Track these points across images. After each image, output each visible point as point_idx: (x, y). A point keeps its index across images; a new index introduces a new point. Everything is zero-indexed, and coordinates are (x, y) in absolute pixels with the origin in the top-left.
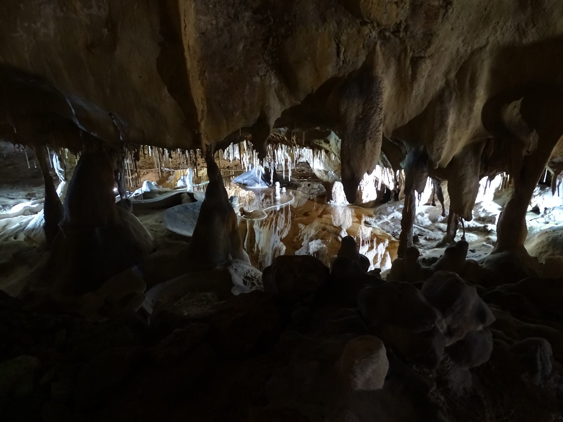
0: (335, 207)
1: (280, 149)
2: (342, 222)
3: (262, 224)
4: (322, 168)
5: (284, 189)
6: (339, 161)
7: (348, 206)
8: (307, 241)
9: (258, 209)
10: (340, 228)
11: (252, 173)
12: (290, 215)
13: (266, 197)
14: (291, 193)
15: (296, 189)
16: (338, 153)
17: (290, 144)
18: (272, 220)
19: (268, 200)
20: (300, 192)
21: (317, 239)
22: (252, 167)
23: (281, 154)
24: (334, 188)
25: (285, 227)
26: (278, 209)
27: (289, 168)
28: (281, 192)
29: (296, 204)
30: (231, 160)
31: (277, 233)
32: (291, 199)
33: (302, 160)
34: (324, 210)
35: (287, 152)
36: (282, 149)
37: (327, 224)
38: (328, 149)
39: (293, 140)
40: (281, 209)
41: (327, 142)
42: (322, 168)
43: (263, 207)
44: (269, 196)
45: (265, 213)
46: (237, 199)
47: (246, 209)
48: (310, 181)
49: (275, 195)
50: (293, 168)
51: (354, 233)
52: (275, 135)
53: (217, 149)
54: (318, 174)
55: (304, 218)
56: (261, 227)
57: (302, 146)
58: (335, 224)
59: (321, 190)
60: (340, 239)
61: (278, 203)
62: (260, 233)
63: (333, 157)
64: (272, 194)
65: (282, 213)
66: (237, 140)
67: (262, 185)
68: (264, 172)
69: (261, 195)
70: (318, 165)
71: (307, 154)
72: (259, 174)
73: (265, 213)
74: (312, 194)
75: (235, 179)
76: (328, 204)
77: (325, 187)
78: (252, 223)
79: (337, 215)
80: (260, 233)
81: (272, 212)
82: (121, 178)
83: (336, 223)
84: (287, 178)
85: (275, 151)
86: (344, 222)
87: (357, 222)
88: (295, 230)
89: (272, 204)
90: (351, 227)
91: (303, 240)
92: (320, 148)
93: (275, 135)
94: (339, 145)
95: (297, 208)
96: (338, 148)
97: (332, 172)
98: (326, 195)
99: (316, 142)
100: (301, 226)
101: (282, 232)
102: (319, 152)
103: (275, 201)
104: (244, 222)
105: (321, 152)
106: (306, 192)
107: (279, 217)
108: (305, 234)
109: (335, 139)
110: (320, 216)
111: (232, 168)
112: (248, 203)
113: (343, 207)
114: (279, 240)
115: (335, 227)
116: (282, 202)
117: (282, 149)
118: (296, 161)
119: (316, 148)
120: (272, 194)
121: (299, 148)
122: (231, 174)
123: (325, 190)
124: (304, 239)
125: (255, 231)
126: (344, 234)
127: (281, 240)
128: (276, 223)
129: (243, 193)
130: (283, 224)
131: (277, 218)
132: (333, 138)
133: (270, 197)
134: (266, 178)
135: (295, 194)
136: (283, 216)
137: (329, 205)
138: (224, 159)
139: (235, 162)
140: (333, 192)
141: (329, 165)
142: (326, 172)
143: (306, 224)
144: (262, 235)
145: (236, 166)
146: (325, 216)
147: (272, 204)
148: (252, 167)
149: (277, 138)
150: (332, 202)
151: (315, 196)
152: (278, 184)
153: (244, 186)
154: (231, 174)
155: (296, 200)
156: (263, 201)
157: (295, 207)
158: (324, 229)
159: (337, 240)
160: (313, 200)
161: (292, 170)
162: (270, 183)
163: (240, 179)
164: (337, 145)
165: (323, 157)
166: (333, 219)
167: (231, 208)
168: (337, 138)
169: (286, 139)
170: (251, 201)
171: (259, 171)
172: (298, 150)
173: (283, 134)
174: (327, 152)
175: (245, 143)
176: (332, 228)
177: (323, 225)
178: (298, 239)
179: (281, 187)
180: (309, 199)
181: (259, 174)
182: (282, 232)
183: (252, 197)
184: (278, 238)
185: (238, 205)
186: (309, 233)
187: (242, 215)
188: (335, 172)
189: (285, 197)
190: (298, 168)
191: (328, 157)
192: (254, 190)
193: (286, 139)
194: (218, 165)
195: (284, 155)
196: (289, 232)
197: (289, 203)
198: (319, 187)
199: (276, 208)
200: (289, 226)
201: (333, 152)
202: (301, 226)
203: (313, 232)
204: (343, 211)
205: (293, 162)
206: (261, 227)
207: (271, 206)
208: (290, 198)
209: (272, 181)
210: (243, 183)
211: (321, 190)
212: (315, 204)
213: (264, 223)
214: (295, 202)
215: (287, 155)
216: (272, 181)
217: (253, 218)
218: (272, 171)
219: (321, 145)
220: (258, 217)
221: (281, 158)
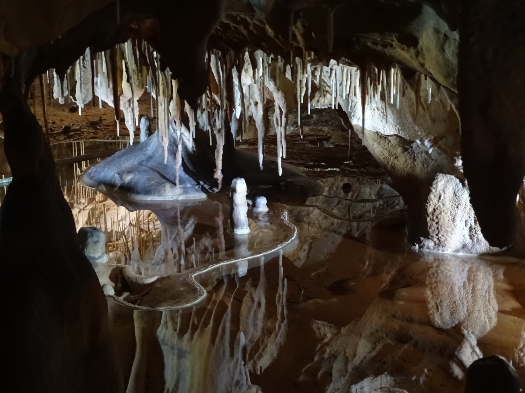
0: (440, 260)
1: (248, 65)
2: (462, 314)
3: (187, 324)
4: (389, 129)
5: (262, 203)
6: (451, 105)
7: (482, 256)
8: (343, 380)
9: (173, 271)
10: (456, 335)
11: (150, 150)
12: (282, 292)
13: (200, 231)
14: (285, 215)
15: (302, 203)
16: (447, 76)
17: (283, 51)
18: (223, 307)
19: (207, 241)
20: (317, 211)
21: (377, 373)
22: (150, 131)
23: (252, 84)
24: (433, 198)
25: (268, 332)
26: (243, 270)
27: (280, 131)
28: (251, 214)
29: (303, 255)
30: (81, 105)
31: (239, 354)
32: (286, 238)
33: (322, 102)
34: (400, 271)
35: (273, 77)
36: (255, 66)
37: (410, 320)
38: (414, 64)
39: (294, 35)
40: (254, 271)
41: (411, 41)
42: (389, 129)
43: (189, 266)
44: (210, 225)
45: (199, 287)
46: (103, 238)
47: (131, 271)
48: (351, 174)
49: (231, 223)
50: (291, 129)
51: (509, 350)
52: (234, 19)
53: (38, 69)
54: (377, 149)
55: (334, 300)
56: (182, 333)
57: (323, 58)
58: (438, 321)
59: (389, 203)
60: (457, 372)
61: (243, 250)
62: (181, 355)
63: (428, 88)
64: (220, 221)
65: (255, 286)
66: (105, 43)
67: (185, 191)
68: (190, 145)
69: (184, 225)
70: (374, 120)
71: (340, 82)
72: (173, 153)
73: (199, 287)
74: (360, 218)
75: (85, 175)
76: (413, 253)
77: (403, 194)
78: (152, 321)
79: (444, 290)
80: (181, 355)
81: (220, 282)
82: (166, 231)
83: (442, 318)
84: (271, 165)
85: (235, 74)
86: (470, 314)
87: (514, 312)
88: (301, 345)
89: (222, 253)
90: (495, 329)
91: (329, 374)
92: (386, 63)
93: (234, 19)
94: (451, 51)
95: (307, 268)
96: (447, 62)
97: (426, 143)
98: (413, 221)
99: (372, 40)
100: (324, 330)
101: (253, 351)
102: (383, 75)
103: (232, 245)
104: (124, 316)
105: (388, 76)
106: (335, 211)
107: (246, 300)
108: (334, 357)
109: (437, 31)
110: (388, 294)
111: (79, 133)
112: (135, 254)
113: (464, 261)
114: (246, 380)
115: (440, 330)
116: (254, 245)
117: (255, 66)
118: (304, 107)
119: (370, 65)
120: (220, 221)
121: (313, 62)
122: (75, 154)
123: (400, 203)
124: (335, 373)
125: (165, 349)
126: (470, 354)
127: (255, 378)
128: (236, 319)
129: (119, 218)
130: (260, 324)
131: (238, 301)
132: (431, 27)
133: (212, 231)
134: (199, 164)
135: (297, 220)
136: (260, 295)
137: (420, 255)
138: (56, 103)
139: (93, 111)
140: (430, 210)
141: (415, 117)
142: (405, 144)
143: (338, 322)
144: (187, 363)
145: (93, 124)
146: (404, 293)
147: (222, 253)
148: (150, 131)
149: (241, 28)
150: (430, 244)
151: (368, 226)
152: (241, 186)
153: (123, 194)
154: (75, 154)
155: (302, 240)
156: (188, 243)
157: (299, 264)
158: (402, 338)
159: (450, 375)
160: (361, 239)
161: (288, 138)
162: (214, 183)
163: (109, 171)
164: (442, 50)
165: (393, 91)
166: (431, 304)
167: (87, 269)
168: (444, 27)
169: (270, 31)
170: (146, 244)
171: (174, 144)
172: (309, 67)
173: (260, 15)
174: (410, 76)
175: (127, 46)
176: (431, 333)
177: (396, 325)
178: (312, 372)
179: (252, 196)
180: (348, 236)
181: (173, 153)
182: (253, 351)
183: (149, 233)
184: (243, 372)
185: (105, 259)
186: (349, 352)
187: (118, 293)
188: (435, 142)
189: (267, 232)
190: (306, 129)
191: (412, 94)
192: (158, 209)
193: (270, 31)
194: (41, 123)
195: (263, 89)
196: (282, 349)
197: (280, 249)
198: (379, 195)
199: (235, 266)
200: (281, 329)
201: (429, 75)
202: (324, 330)
203: (363, 349)
204: (465, 274)
205: (291, 108)
206: (182, 333)
207: (218, 261)
208: (284, 234)
209: (219, 175)
210: (118, 182)
211: (389, 203)
212: (370, 251)
213: (194, 319)
214: (300, 248)
215: (271, 85)
216: (219, 175)
217: (159, 303)
218: (221, 142)
219: (388, 51)
220: (177, 298)
221: (251, 96)
